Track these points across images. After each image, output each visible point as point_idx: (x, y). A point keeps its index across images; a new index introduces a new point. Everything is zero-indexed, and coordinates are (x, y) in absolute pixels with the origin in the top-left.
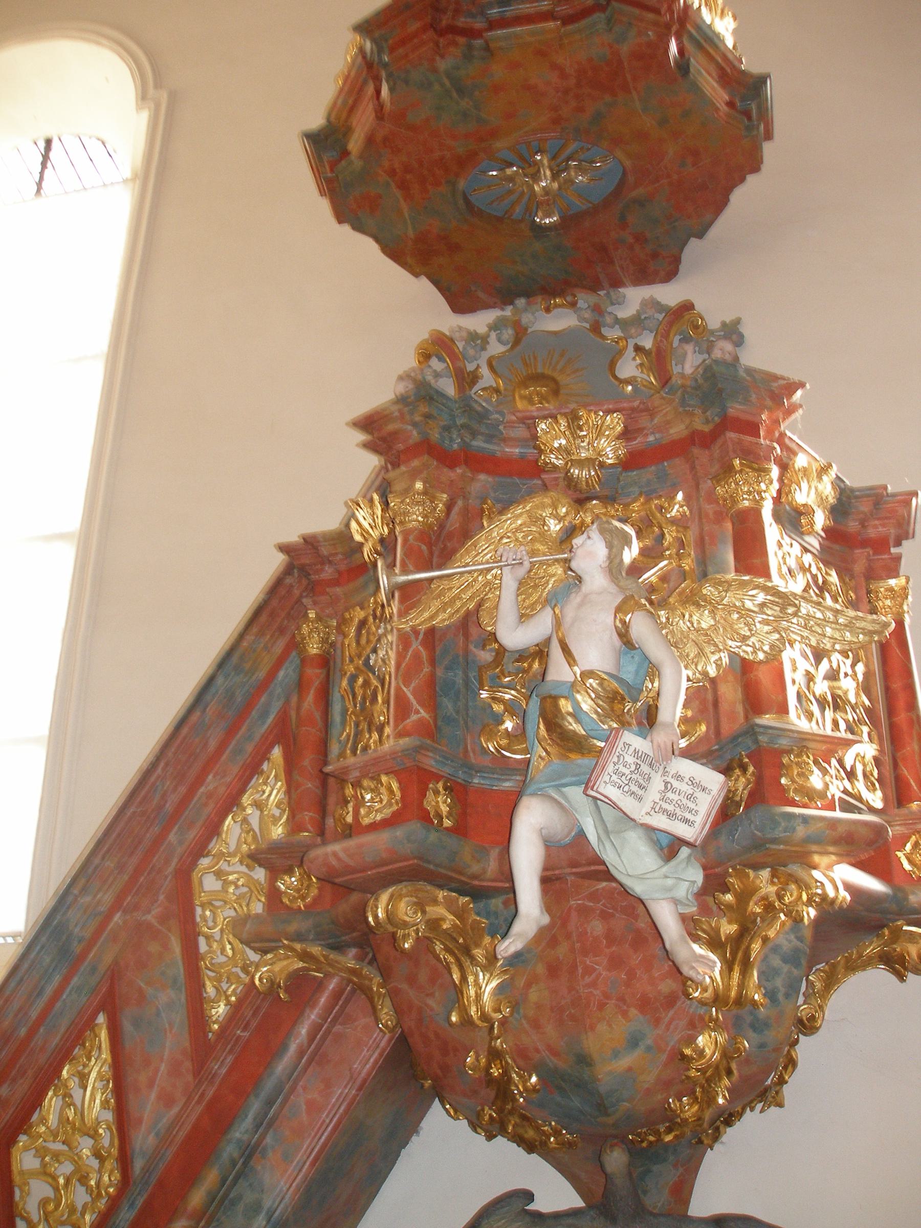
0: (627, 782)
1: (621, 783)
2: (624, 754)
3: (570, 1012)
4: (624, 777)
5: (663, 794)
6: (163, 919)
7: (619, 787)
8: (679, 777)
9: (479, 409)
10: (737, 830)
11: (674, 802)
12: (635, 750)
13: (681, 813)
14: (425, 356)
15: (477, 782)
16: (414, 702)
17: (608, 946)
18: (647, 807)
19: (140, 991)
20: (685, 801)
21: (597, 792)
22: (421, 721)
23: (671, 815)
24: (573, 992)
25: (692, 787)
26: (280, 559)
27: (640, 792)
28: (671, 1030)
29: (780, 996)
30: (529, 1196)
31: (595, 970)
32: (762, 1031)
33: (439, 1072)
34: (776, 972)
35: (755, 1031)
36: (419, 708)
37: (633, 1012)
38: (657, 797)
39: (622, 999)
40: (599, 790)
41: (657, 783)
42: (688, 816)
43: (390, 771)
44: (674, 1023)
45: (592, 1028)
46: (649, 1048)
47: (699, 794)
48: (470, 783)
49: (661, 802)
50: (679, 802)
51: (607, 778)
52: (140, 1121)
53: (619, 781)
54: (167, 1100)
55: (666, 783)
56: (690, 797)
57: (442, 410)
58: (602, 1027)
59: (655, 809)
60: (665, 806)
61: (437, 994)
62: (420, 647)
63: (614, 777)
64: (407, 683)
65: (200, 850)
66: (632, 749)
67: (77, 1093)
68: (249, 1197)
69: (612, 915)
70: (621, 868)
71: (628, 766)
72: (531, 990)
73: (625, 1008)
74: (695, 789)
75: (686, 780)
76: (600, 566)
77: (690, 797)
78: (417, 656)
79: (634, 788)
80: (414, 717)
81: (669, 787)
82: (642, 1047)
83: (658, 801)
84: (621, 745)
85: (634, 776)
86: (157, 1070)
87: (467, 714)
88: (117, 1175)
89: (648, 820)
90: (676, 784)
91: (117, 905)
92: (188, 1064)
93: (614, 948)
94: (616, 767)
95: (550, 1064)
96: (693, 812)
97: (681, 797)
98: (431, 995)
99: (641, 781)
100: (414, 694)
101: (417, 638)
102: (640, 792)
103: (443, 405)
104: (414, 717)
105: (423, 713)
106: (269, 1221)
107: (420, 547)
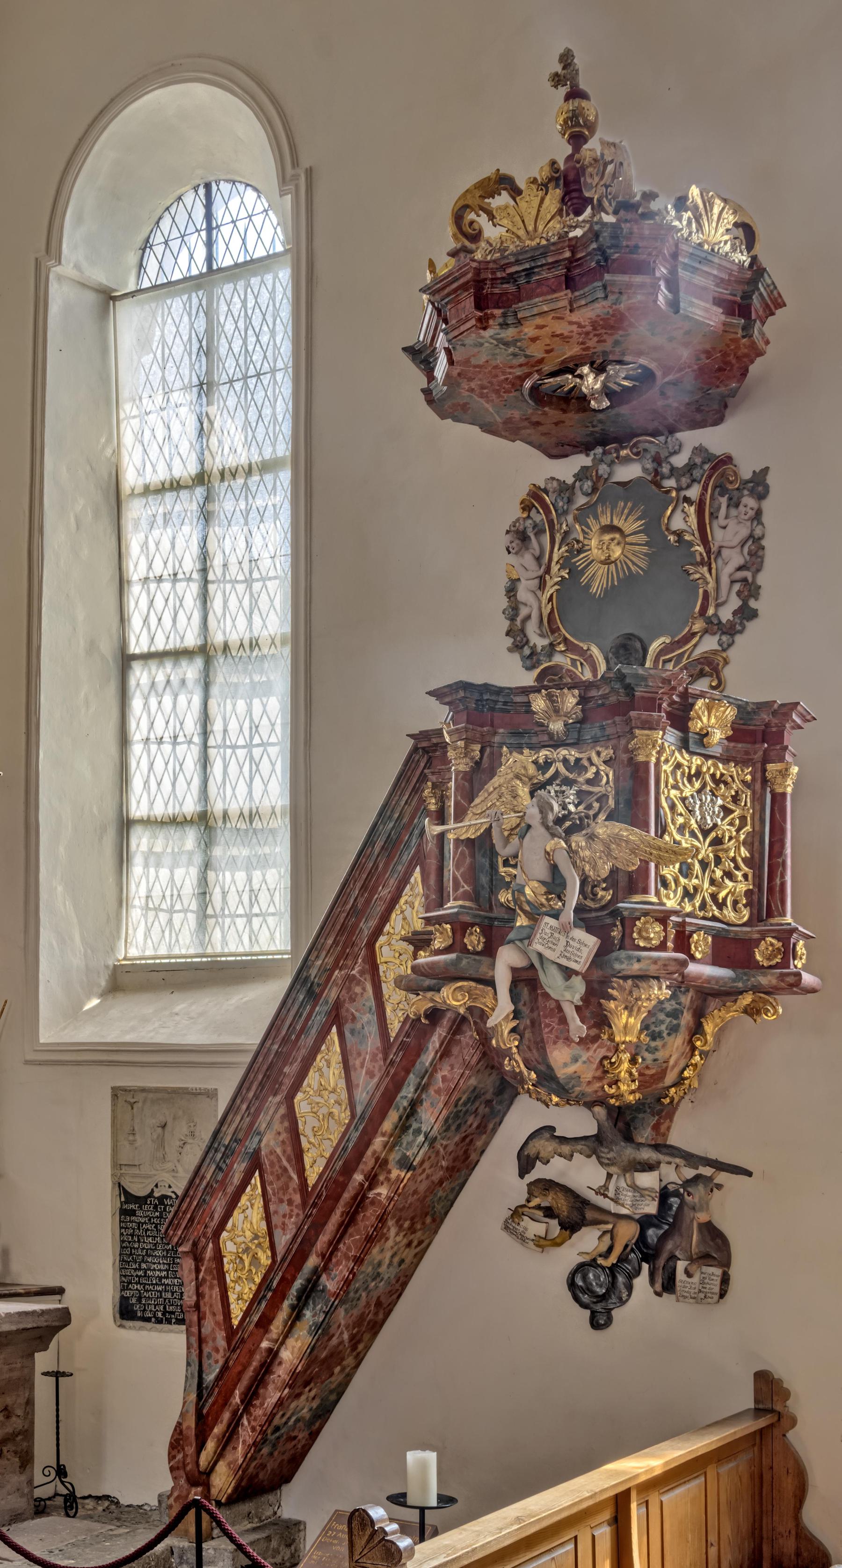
6: (362, 973)
8: (573, 939)
14: (527, 507)
19: (353, 1014)
22: (465, 892)
23: (568, 959)
26: (411, 742)
30: (552, 1129)
41: (563, 940)
46: (584, 1062)
47: (583, 948)
52: (358, 1085)
54: (370, 1074)
59: (562, 955)
65: (378, 931)
67: (325, 1069)
68: (415, 1125)
78: (462, 853)
80: (461, 890)
86: (364, 1059)
88: (348, 1113)
89: (558, 961)
91: (336, 966)
92: (380, 1056)
104: (461, 890)
105: (466, 888)
106: (426, 1138)
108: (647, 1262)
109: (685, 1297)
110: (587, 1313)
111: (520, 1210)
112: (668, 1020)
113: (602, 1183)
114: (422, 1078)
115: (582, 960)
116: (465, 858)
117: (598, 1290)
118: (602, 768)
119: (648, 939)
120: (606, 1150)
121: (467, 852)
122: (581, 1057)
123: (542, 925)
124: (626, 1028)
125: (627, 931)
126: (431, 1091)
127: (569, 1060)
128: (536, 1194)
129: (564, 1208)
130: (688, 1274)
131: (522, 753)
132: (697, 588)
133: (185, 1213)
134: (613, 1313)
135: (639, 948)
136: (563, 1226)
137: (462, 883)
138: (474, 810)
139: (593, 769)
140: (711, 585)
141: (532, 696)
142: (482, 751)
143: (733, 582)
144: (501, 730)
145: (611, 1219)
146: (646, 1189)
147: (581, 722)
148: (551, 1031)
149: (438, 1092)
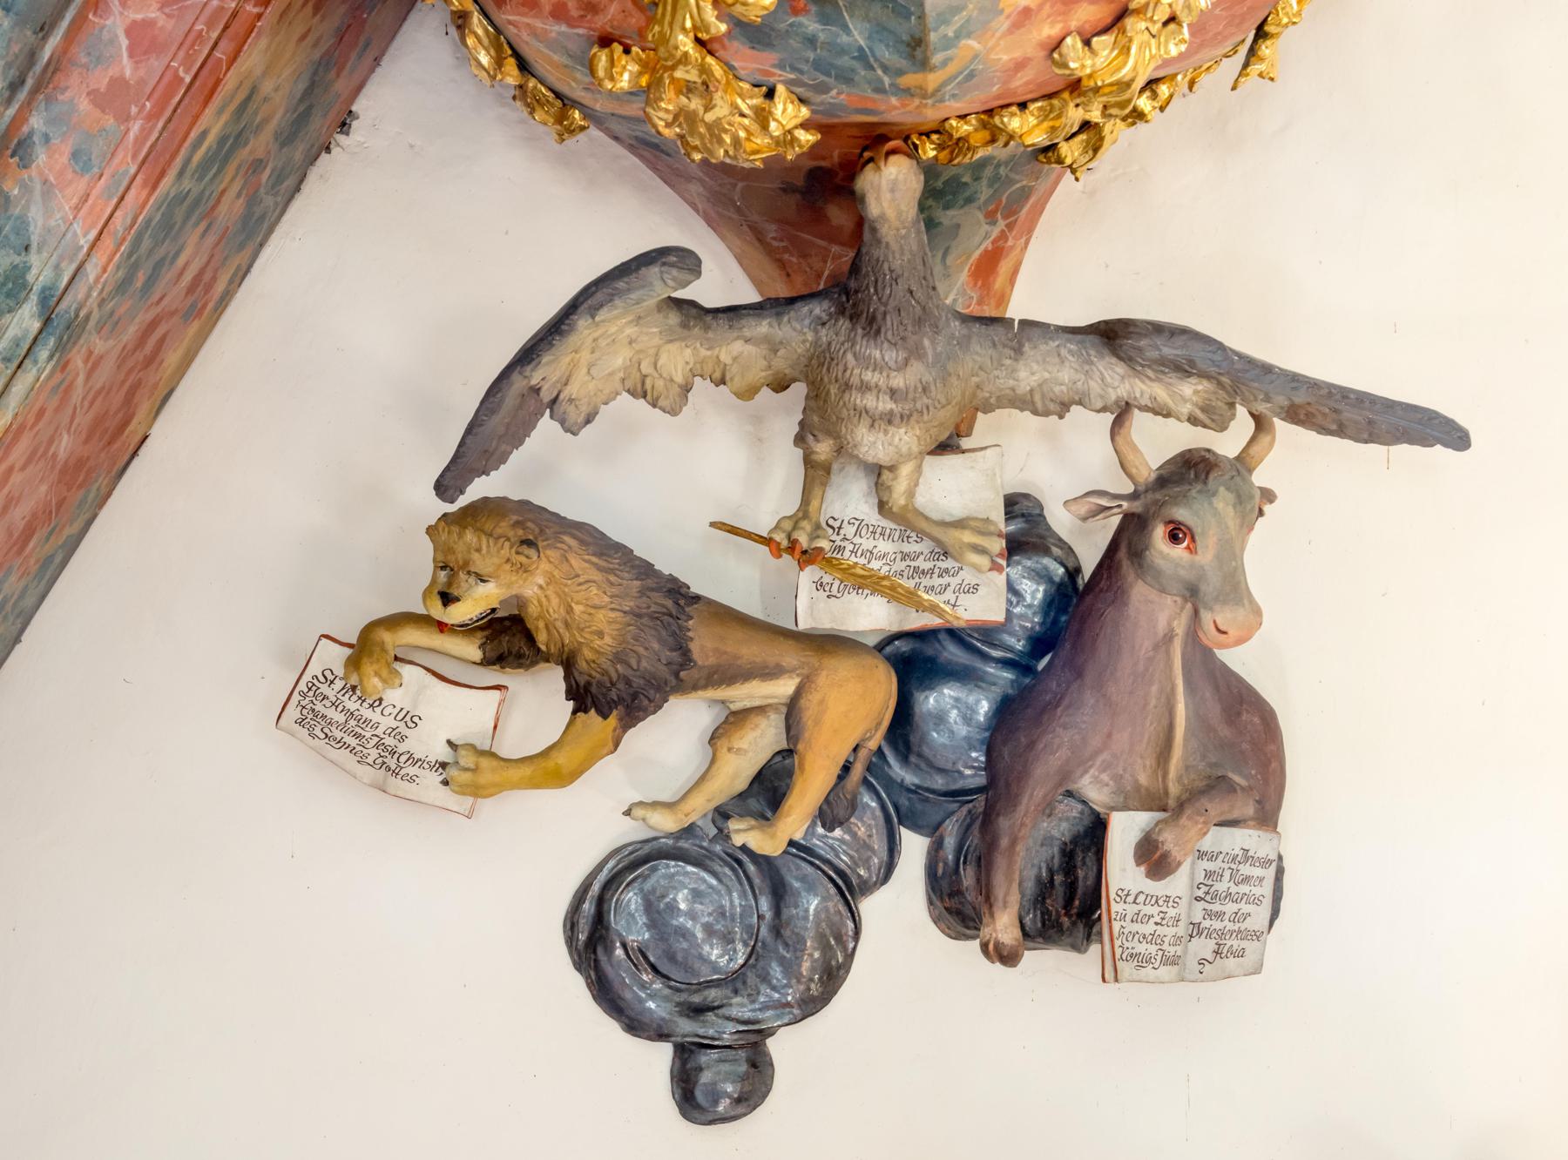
46: (53, 296)
106: (47, 322)
108: (916, 827)
109: (1142, 961)
110: (661, 1056)
111: (386, 637)
113: (791, 506)
114: (44, 30)
117: (714, 953)
120: (891, 356)
126: (76, 95)
128: (480, 564)
129: (602, 619)
130: (1153, 858)
133: (637, 959)
134: (772, 1044)
136: (583, 696)
145: (790, 656)
146: (960, 524)
149: (113, 98)
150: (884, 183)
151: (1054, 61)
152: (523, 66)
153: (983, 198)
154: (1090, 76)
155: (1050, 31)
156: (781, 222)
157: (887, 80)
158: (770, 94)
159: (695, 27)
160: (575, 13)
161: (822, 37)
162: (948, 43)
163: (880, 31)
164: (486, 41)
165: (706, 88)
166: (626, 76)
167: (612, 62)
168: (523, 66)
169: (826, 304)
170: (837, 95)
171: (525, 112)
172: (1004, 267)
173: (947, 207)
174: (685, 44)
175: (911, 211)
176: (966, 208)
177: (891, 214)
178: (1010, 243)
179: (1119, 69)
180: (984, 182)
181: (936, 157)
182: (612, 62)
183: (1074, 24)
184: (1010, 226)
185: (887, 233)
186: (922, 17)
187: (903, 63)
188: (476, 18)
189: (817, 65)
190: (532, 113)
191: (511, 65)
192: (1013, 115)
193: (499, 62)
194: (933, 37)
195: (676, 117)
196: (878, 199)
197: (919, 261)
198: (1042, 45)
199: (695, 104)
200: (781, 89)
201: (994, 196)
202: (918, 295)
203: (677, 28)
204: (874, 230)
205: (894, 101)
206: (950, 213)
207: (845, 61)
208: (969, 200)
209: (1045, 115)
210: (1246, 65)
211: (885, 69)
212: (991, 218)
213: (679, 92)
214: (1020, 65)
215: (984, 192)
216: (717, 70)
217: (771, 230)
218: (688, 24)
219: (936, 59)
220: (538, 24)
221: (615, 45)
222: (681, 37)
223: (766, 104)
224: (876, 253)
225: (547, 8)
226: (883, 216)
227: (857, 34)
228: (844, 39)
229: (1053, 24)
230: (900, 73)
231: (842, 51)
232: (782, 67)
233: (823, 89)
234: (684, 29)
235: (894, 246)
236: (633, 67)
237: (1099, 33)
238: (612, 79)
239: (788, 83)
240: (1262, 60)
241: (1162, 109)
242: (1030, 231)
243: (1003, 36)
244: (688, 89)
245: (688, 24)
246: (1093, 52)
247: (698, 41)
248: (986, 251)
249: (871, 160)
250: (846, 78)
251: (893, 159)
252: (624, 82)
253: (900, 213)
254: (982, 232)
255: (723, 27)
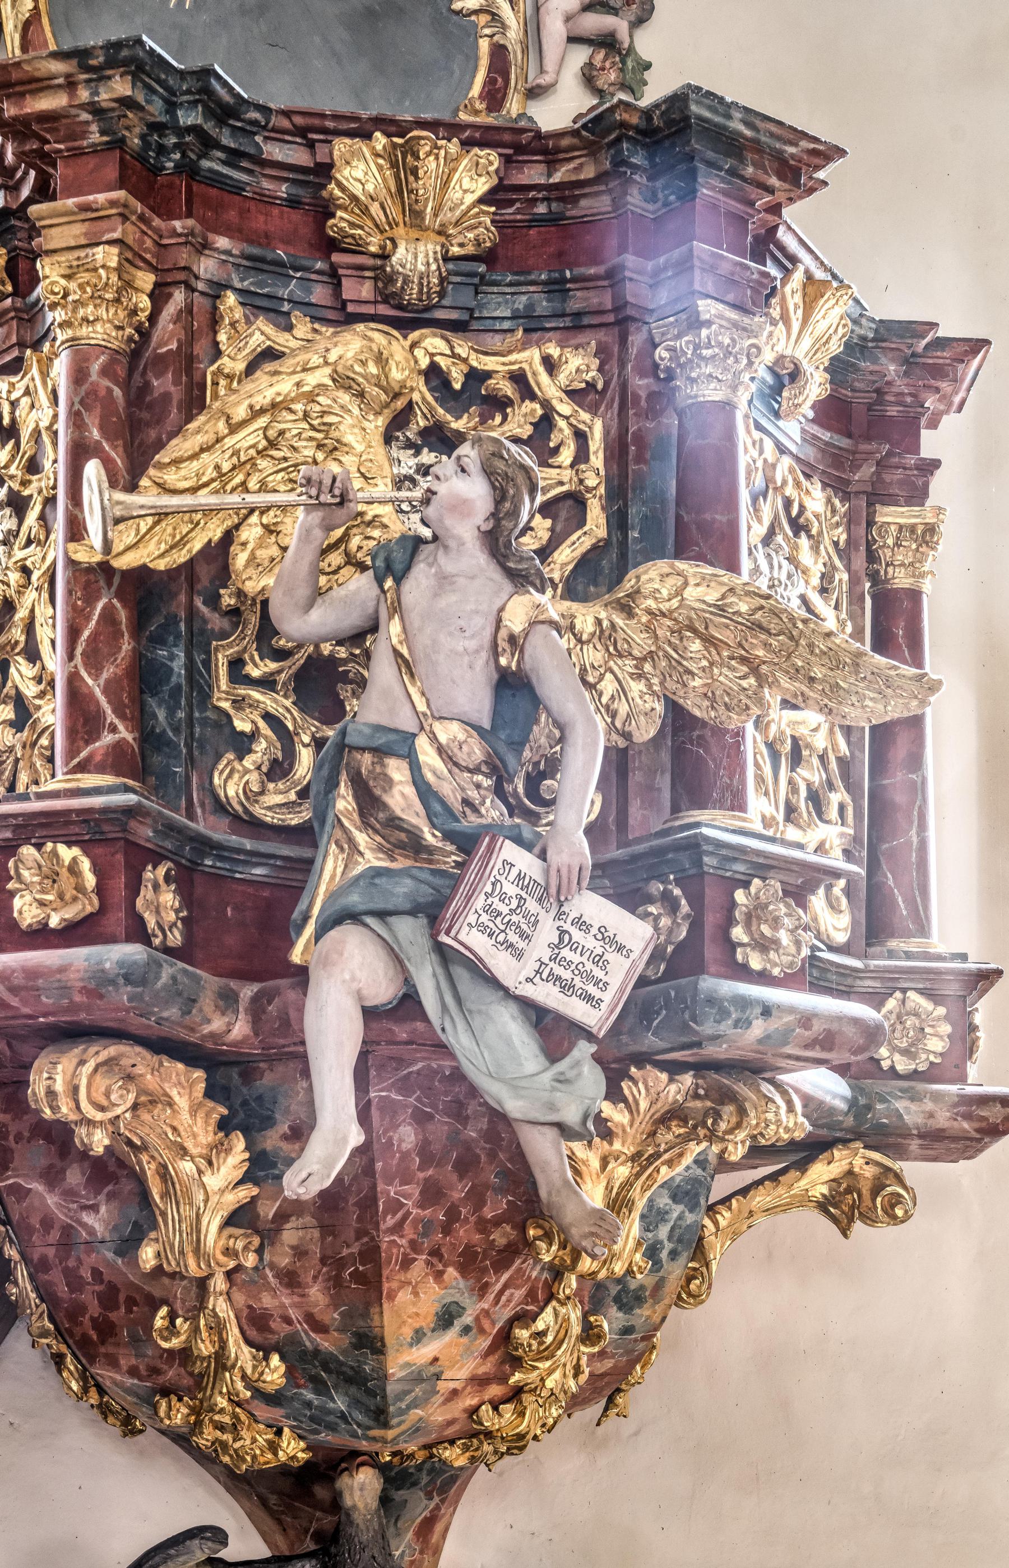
0: (503, 927)
1: (494, 928)
2: (502, 879)
3: (357, 1269)
4: (499, 919)
5: (556, 951)
7: (490, 935)
8: (580, 923)
9: (227, 98)
10: (658, 1014)
11: (573, 967)
12: (519, 874)
13: (581, 985)
15: (210, 863)
16: (109, 711)
17: (421, 1169)
18: (529, 968)
20: (589, 966)
21: (455, 939)
22: (119, 747)
23: (566, 988)
24: (365, 1239)
25: (601, 943)
27: (521, 944)
28: (501, 1303)
29: (664, 1255)
31: (403, 1205)
32: (632, 1309)
33: (94, 1335)
34: (662, 1215)
35: (620, 1309)
36: (116, 721)
37: (451, 1272)
38: (546, 954)
39: (435, 1253)
40: (460, 937)
41: (547, 932)
42: (591, 989)
43: (74, 838)
44: (507, 1293)
45: (391, 1297)
46: (466, 1330)
47: (611, 956)
48: (199, 865)
49: (552, 964)
50: (580, 967)
51: (472, 918)
53: (491, 925)
55: (562, 932)
56: (599, 960)
57: (154, 91)
58: (404, 1296)
60: (558, 971)
61: (103, 1209)
62: (115, 601)
63: (484, 918)
64: (94, 663)
66: (514, 872)
69: (430, 1117)
70: (479, 1062)
71: (507, 901)
72: (288, 1226)
73: (440, 1267)
74: (607, 947)
75: (594, 931)
76: (479, 528)
77: (599, 960)
79: (513, 938)
80: (108, 739)
81: (566, 941)
82: (458, 1325)
83: (547, 961)
84: (499, 864)
85: (515, 918)
87: (192, 734)
89: (528, 991)
90: (577, 935)
93: (430, 1172)
94: (489, 902)
95: (308, 1344)
96: (601, 985)
97: (584, 959)
98: (94, 1208)
99: (524, 927)
100: (105, 692)
101: (110, 585)
102: (521, 944)
103: (158, 81)
104: (108, 739)
107: (110, 391)
112: (677, 1209)
115: (608, 997)
116: (118, 635)
118: (565, 408)
119: (764, 945)
121: (123, 615)
122: (461, 1310)
123: (497, 862)
124: (505, 1234)
125: (711, 919)
127: (428, 1321)
131: (289, 328)
132: (473, 34)
135: (743, 972)
137: (111, 717)
138: (171, 477)
139: (534, 409)
140: (514, 33)
141: (341, 146)
142: (159, 296)
143: (573, 40)
144: (222, 242)
147: (489, 257)
148: (397, 1228)
150: (355, 1484)
151: (474, 1421)
152: (101, 1391)
153: (423, 1482)
154: (498, 1430)
155: (471, 1401)
156: (280, 1494)
157: (360, 1432)
158: (279, 1433)
159: (229, 1392)
160: (144, 1373)
161: (316, 1403)
162: (402, 1412)
163: (355, 1403)
164: (76, 1375)
165: (235, 1429)
166: (179, 1416)
167: (170, 1408)
168: (101, 1391)
169: (314, 1562)
170: (324, 1437)
171: (100, 1417)
172: (439, 1527)
173: (398, 1489)
174: (222, 1402)
175: (374, 1504)
176: (412, 1490)
177: (361, 1505)
178: (443, 1511)
179: (518, 1426)
180: (425, 1472)
181: (391, 1461)
182: (170, 1408)
183: (486, 1398)
184: (443, 1501)
185: (358, 1518)
186: (384, 1397)
187: (371, 1423)
188: (69, 1358)
189: (312, 1419)
190: (105, 1418)
191: (93, 1393)
192: (446, 1448)
193: (85, 1390)
194: (392, 1409)
195: (213, 1443)
196: (352, 1495)
197: (379, 1536)
198: (465, 1410)
199: (227, 1437)
200: (286, 1430)
201: (432, 1481)
202: (379, 1559)
203: (216, 1391)
204: (348, 1515)
205: (364, 1443)
206: (401, 1492)
207: (331, 1418)
208: (415, 1484)
209: (466, 1448)
210: (606, 1409)
211: (359, 1425)
212: (429, 1496)
213: (216, 1428)
214: (450, 1423)
215: (425, 1479)
216: (243, 1417)
217: (273, 1499)
218: (225, 1390)
219: (394, 1422)
220: (118, 1377)
221: (172, 1396)
222: (219, 1399)
223: (276, 1439)
224: (352, 1531)
225: (125, 1368)
226: (354, 1507)
227: (340, 1404)
228: (332, 1405)
229: (473, 1397)
230: (369, 1428)
231: (330, 1412)
232: (287, 1417)
233: (317, 1432)
234: (221, 1393)
235: (362, 1526)
236: (185, 1411)
237: (504, 1402)
238: (170, 1418)
239: (291, 1428)
240: (617, 1406)
241: (549, 1431)
242: (457, 1502)
243: (440, 1406)
244: (221, 1427)
245: (225, 1390)
246: (500, 1415)
247: (230, 1400)
248: (425, 1518)
249: (346, 1469)
250: (332, 1428)
251: (362, 1469)
252: (178, 1419)
253: (366, 1505)
254: (423, 1505)
255: (249, 1394)
